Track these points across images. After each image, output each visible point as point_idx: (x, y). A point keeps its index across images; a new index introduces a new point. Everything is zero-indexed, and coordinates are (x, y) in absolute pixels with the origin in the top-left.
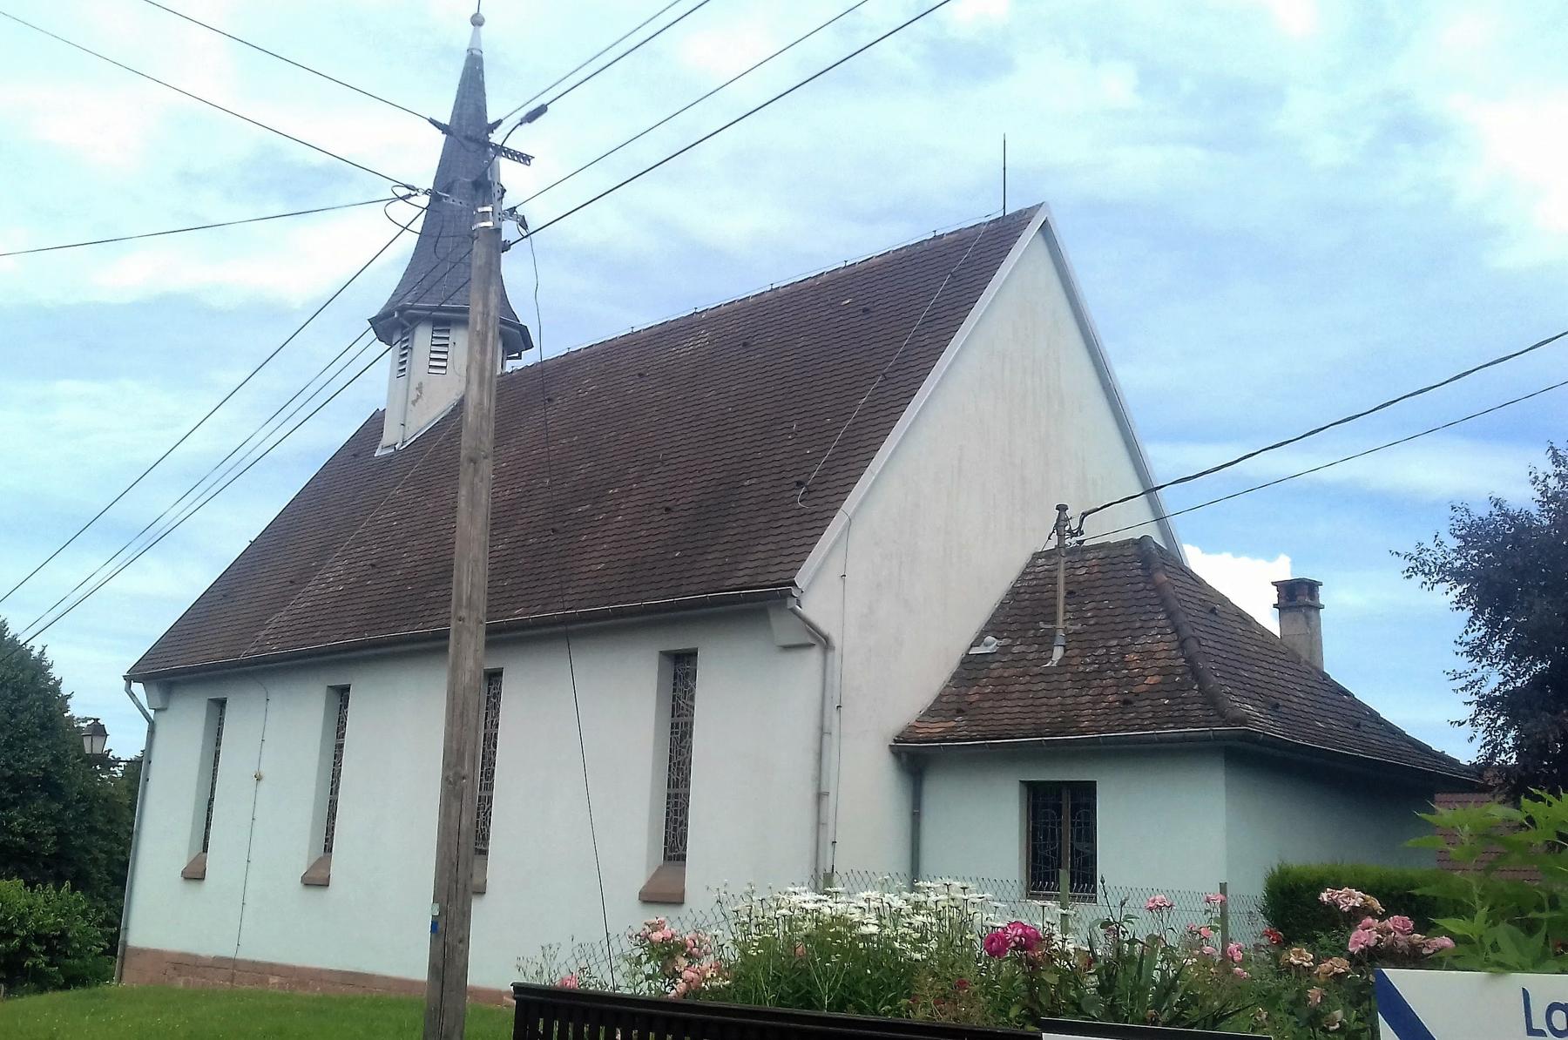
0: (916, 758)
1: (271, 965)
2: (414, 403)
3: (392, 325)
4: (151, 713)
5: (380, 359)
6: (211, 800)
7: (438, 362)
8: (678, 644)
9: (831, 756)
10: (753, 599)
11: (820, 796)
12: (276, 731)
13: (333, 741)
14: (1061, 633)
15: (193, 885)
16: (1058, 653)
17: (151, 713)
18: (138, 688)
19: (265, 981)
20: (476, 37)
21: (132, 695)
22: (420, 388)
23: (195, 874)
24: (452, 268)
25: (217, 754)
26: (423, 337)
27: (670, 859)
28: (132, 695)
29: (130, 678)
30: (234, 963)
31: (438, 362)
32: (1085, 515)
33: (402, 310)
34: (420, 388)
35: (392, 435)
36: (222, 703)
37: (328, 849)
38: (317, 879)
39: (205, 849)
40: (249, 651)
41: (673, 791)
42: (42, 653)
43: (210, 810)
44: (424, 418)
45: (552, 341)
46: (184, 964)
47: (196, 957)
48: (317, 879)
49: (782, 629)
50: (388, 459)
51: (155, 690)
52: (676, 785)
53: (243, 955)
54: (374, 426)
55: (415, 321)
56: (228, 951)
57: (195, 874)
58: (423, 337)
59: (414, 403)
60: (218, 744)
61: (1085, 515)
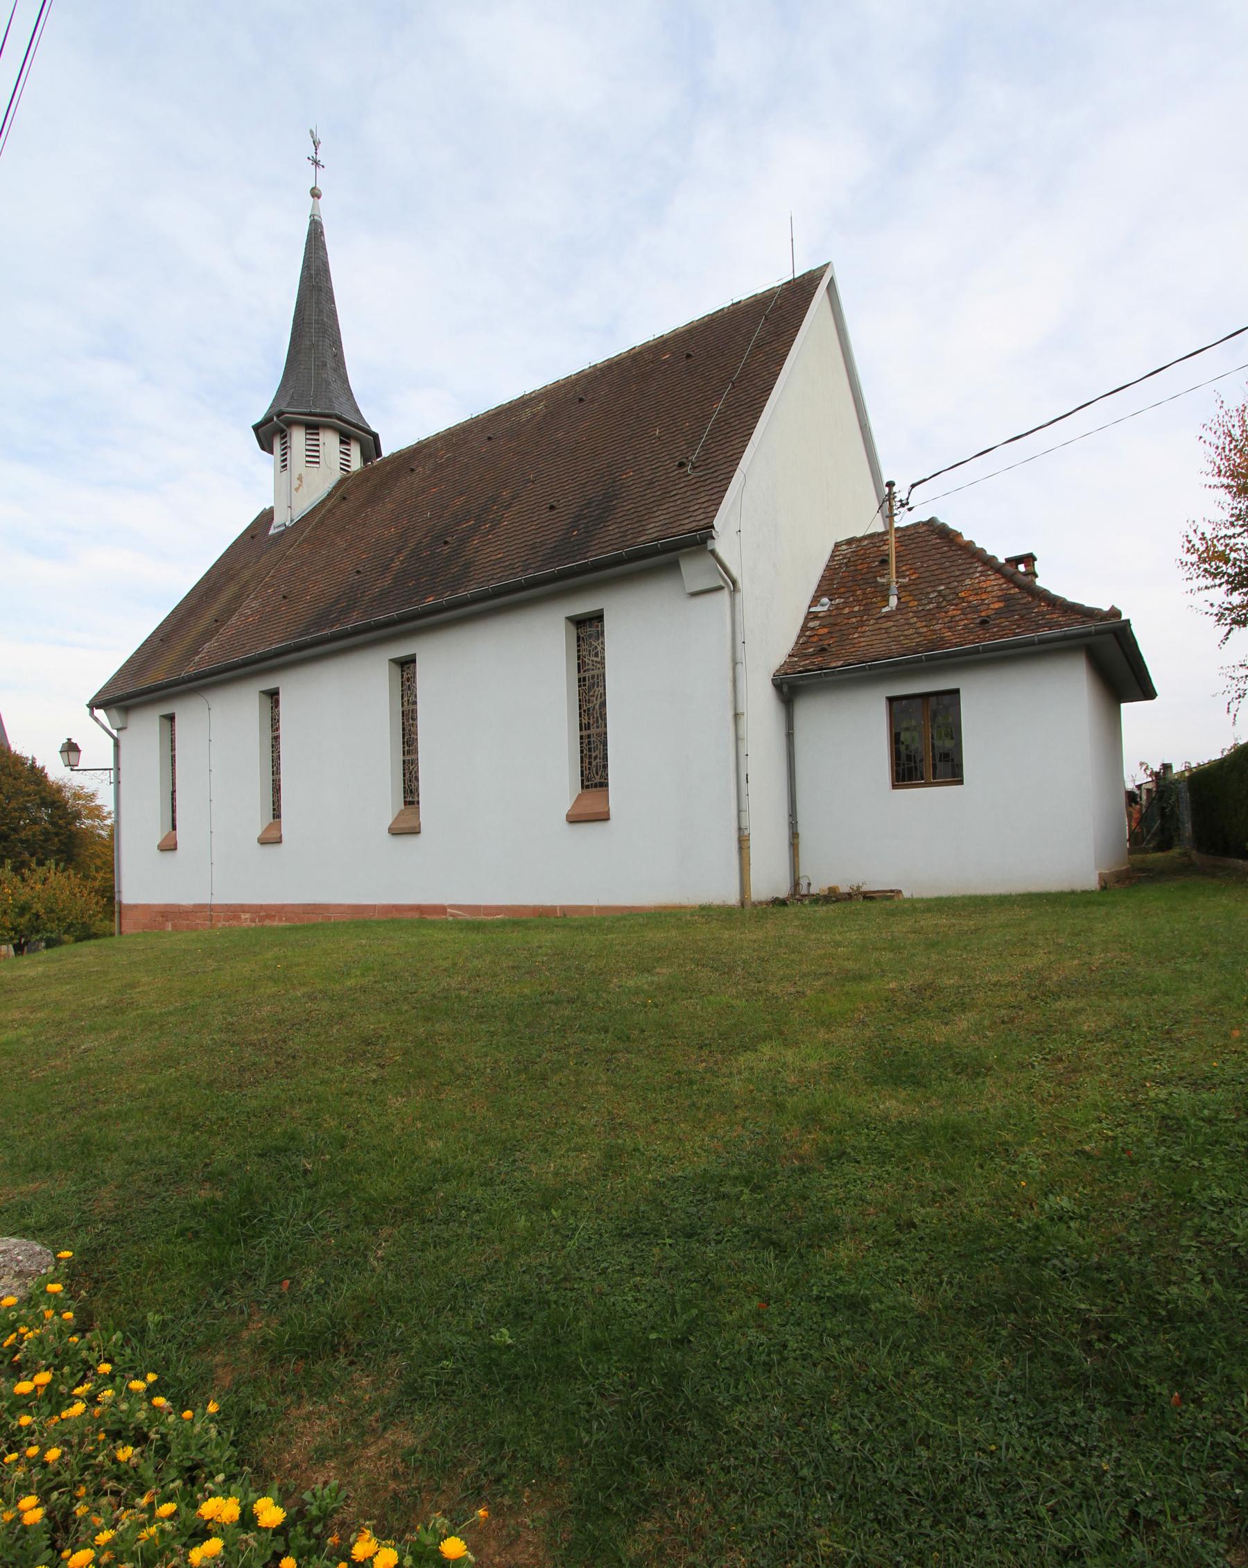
0: (790, 688)
1: (242, 906)
2: (297, 490)
3: (269, 433)
4: (115, 732)
5: (266, 464)
6: (174, 792)
7: (313, 457)
8: (582, 607)
9: (740, 685)
10: (673, 547)
11: (737, 716)
12: (221, 727)
13: (269, 735)
14: (894, 586)
15: (168, 855)
16: (893, 601)
17: (115, 732)
18: (100, 713)
19: (238, 918)
20: (314, 206)
21: (96, 720)
22: (300, 479)
23: (168, 846)
24: (310, 396)
25: (173, 757)
26: (298, 437)
27: (588, 787)
28: (96, 720)
29: (93, 705)
30: (211, 907)
31: (313, 457)
32: (913, 486)
33: (280, 414)
34: (300, 479)
35: (282, 519)
36: (171, 718)
37: (277, 814)
38: (271, 838)
39: (174, 828)
40: (191, 670)
41: (585, 733)
42: (37, 1506)
43: (173, 799)
44: (306, 501)
45: (395, 439)
46: (168, 914)
47: (179, 906)
48: (271, 838)
49: (694, 572)
50: (281, 534)
51: (114, 713)
52: (588, 727)
53: (216, 901)
54: (266, 517)
55: (291, 423)
56: (205, 900)
57: (168, 846)
58: (298, 437)
59: (297, 490)
60: (173, 749)
61: (913, 486)
